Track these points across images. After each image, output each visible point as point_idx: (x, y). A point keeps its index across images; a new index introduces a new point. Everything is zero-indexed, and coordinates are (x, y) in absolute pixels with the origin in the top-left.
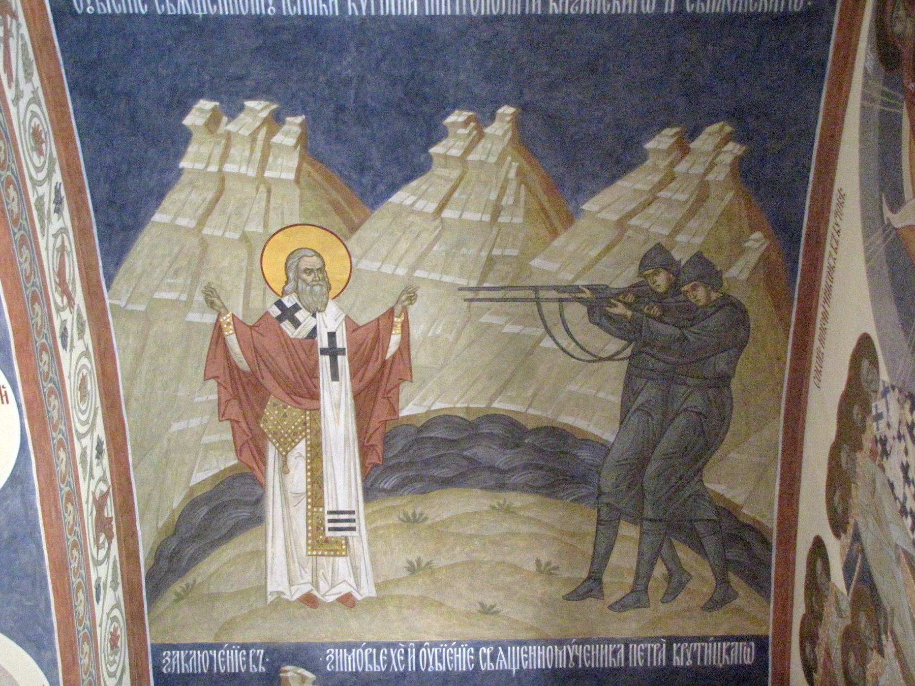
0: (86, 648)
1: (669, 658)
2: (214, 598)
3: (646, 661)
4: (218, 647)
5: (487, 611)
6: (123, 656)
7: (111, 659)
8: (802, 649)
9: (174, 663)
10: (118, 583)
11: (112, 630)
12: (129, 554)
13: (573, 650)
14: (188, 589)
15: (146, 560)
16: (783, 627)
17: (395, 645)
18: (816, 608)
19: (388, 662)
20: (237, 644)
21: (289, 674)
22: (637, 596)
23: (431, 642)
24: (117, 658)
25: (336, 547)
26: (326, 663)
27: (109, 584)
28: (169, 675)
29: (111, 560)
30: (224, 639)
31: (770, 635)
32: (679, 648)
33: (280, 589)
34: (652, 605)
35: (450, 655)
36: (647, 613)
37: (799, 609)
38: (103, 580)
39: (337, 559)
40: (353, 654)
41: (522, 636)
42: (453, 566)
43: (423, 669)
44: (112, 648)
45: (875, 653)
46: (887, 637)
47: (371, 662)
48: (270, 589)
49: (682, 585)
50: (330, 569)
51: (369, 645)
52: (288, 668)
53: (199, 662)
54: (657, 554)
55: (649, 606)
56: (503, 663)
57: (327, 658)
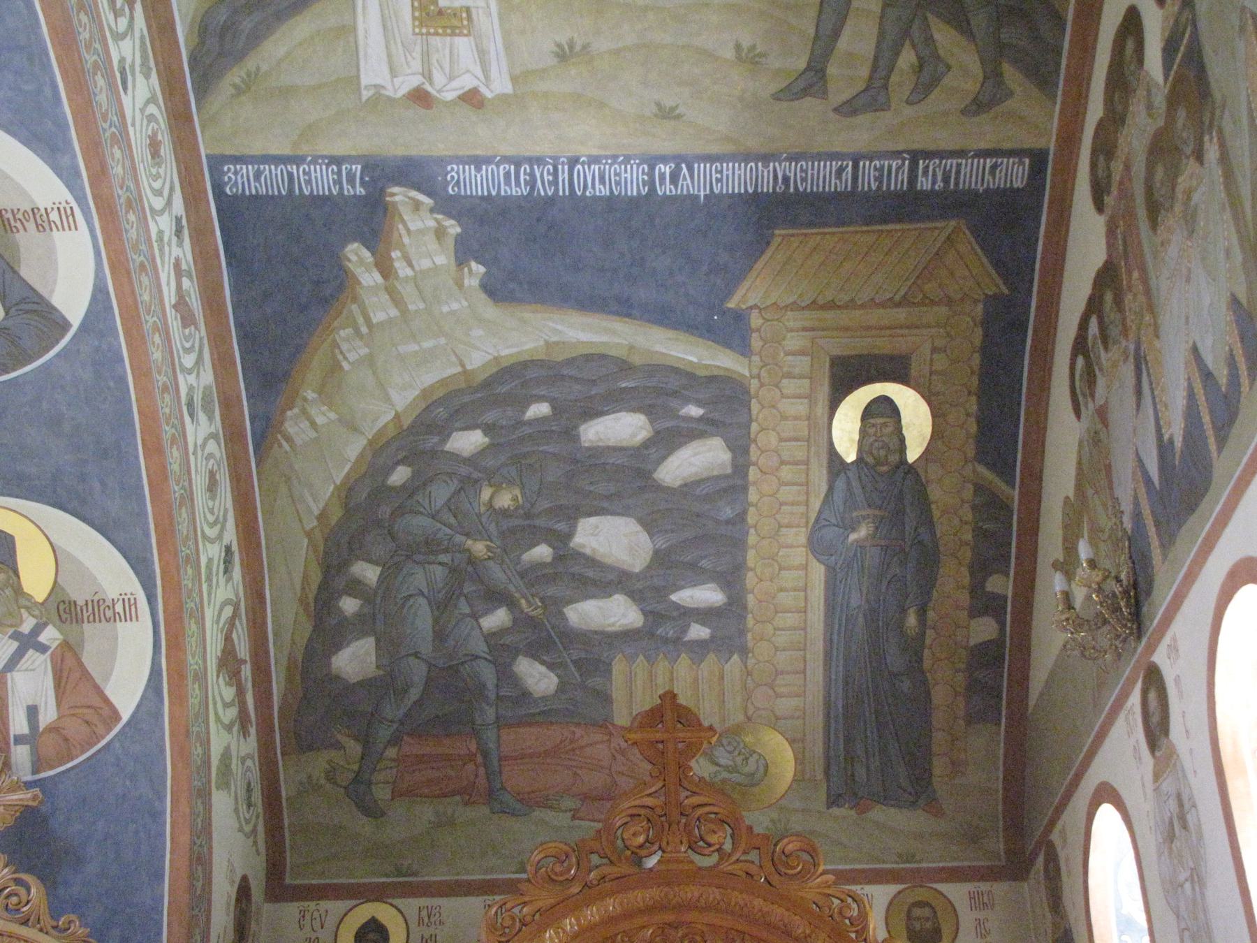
0: (118, 154)
1: (913, 179)
2: (287, 92)
3: (881, 182)
4: (298, 160)
5: (667, 114)
6: (169, 170)
7: (154, 171)
8: (1094, 166)
9: (240, 181)
10: (150, 69)
11: (150, 132)
12: (161, 27)
13: (782, 168)
14: (252, 79)
15: (186, 41)
16: (1069, 139)
17: (540, 161)
18: (1119, 108)
19: (532, 183)
20: (323, 157)
21: (397, 198)
22: (872, 96)
23: (589, 156)
24: (162, 171)
25: (455, 22)
26: (447, 183)
27: (138, 69)
28: (235, 197)
29: (137, 35)
30: (304, 149)
31: (1010, 595)
32: (927, 167)
33: (379, 81)
34: (893, 106)
35: (616, 174)
36: (887, 117)
37: (1095, 110)
38: (129, 61)
39: (456, 39)
40: (484, 172)
41: (714, 149)
42: (617, 52)
43: (579, 194)
44: (153, 157)
45: (1192, 161)
46: (1211, 140)
47: (508, 183)
48: (365, 80)
49: (934, 82)
50: (447, 51)
51: (506, 159)
52: (396, 189)
53: (273, 180)
54: (906, 33)
55: (889, 108)
56: (687, 185)
57: (449, 178)
